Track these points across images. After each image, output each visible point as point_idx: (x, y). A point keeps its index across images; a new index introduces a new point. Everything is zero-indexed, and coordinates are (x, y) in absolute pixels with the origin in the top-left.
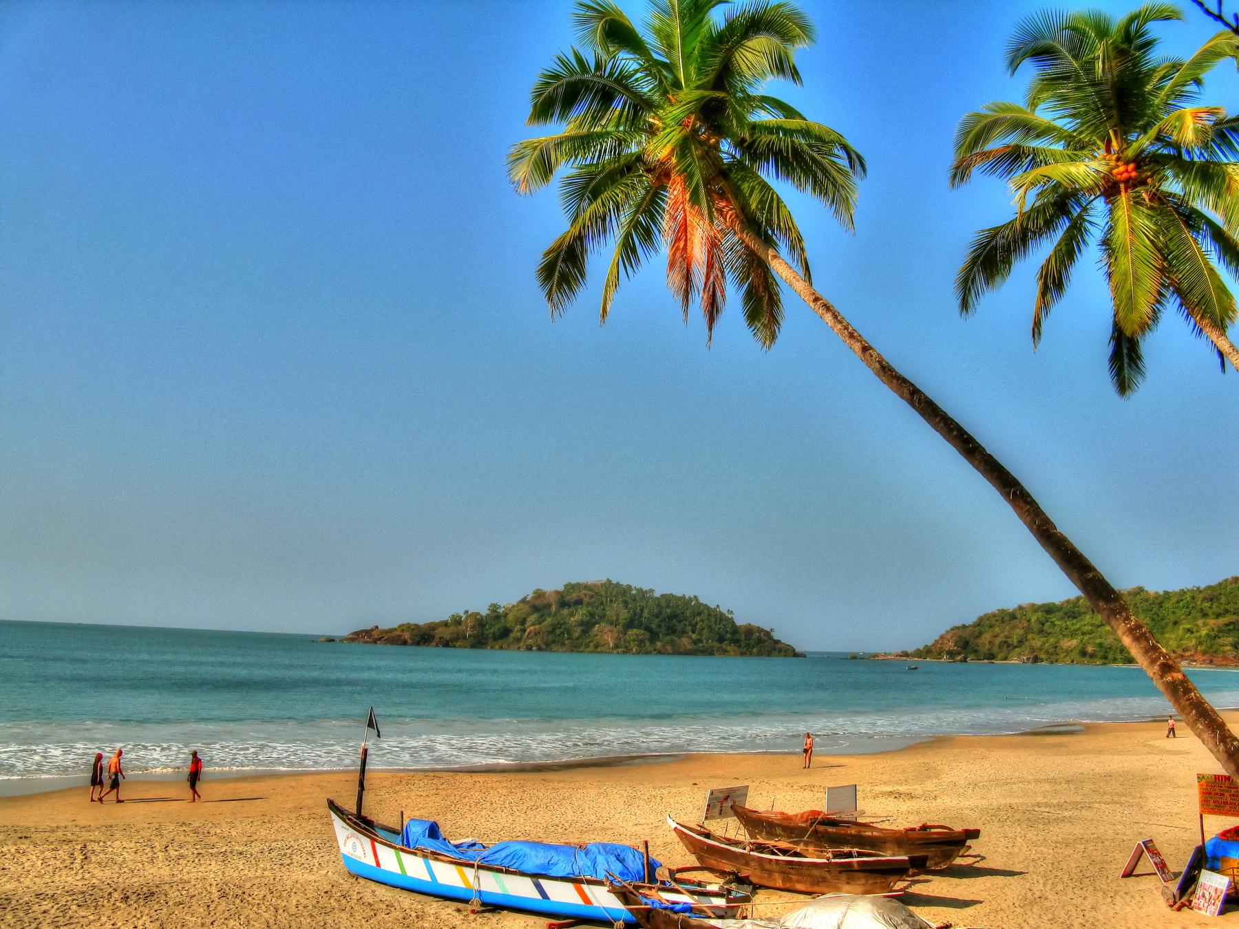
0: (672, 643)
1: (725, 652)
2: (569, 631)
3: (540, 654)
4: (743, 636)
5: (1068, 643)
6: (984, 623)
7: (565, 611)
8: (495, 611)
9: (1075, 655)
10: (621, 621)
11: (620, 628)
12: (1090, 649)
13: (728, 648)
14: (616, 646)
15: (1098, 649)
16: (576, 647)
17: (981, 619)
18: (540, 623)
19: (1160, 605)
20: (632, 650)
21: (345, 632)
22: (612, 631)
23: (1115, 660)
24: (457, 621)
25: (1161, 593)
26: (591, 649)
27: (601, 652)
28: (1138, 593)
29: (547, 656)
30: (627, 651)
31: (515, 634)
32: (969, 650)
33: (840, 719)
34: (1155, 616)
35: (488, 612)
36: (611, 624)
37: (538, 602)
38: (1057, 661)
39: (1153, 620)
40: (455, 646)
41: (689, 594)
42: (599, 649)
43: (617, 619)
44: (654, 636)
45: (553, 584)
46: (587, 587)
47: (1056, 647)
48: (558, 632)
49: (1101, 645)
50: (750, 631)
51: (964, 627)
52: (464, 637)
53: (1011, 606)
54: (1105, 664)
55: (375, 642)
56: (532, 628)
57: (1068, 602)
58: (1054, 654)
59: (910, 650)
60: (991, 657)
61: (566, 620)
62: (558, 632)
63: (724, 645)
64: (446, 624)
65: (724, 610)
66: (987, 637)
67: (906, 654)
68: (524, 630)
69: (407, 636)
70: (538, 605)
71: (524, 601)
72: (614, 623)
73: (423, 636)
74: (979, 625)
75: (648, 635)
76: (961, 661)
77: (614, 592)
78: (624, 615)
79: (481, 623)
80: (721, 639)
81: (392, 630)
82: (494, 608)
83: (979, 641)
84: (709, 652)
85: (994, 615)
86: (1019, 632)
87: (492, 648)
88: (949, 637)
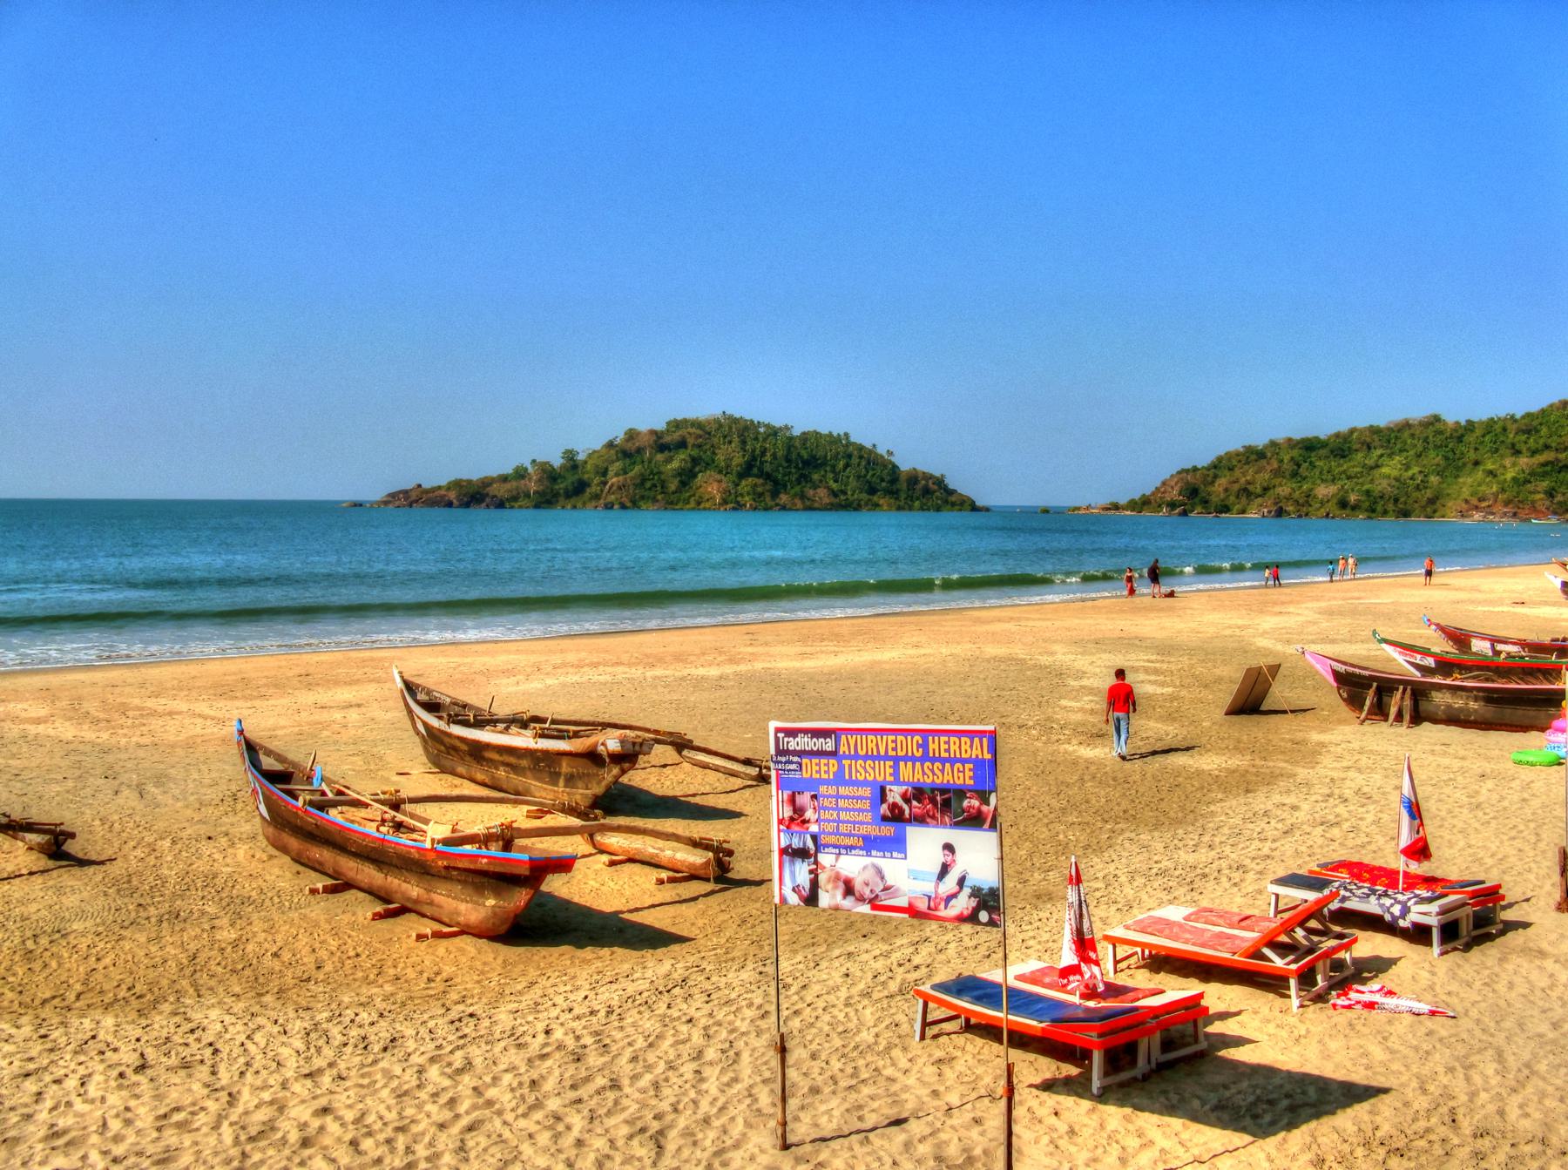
0: (803, 497)
1: (876, 506)
2: (663, 484)
3: (623, 513)
4: (904, 486)
5: (1323, 491)
6: (1220, 465)
7: (660, 457)
8: (572, 459)
9: (1332, 507)
10: (736, 469)
11: (733, 477)
12: (1353, 498)
13: (881, 502)
14: (725, 502)
15: (1363, 498)
16: (672, 503)
17: (1220, 459)
18: (626, 473)
19: (1460, 439)
20: (745, 505)
21: (376, 493)
22: (720, 481)
23: (1385, 513)
24: (521, 474)
25: (1463, 423)
26: (692, 504)
27: (705, 509)
28: (1432, 424)
29: (631, 514)
30: (739, 507)
31: (594, 489)
32: (1197, 500)
33: (436, 590)
34: (1450, 455)
35: (562, 461)
36: (720, 472)
37: (630, 446)
38: (1307, 515)
39: (1447, 458)
40: (512, 507)
41: (837, 430)
42: (702, 506)
43: (728, 466)
44: (777, 487)
45: (651, 417)
46: (697, 424)
47: (1308, 496)
48: (648, 485)
49: (1368, 493)
50: (914, 478)
51: (1195, 469)
52: (527, 495)
53: (1260, 441)
54: (1369, 518)
55: (411, 506)
56: (614, 480)
57: (1337, 435)
58: (1304, 506)
59: (1123, 501)
60: (1225, 509)
61: (662, 469)
62: (648, 485)
63: (875, 498)
64: (504, 479)
65: (882, 450)
66: (1222, 482)
67: (1116, 507)
68: (605, 483)
69: (452, 495)
70: (627, 451)
71: (610, 445)
72: (725, 470)
73: (473, 495)
74: (1215, 467)
75: (769, 486)
76: (1180, 514)
77: (742, 430)
78: (738, 460)
79: (549, 474)
80: (872, 491)
81: (433, 490)
82: (570, 455)
83: (1211, 489)
84: (857, 507)
85: (1238, 454)
86: (1265, 476)
87: (563, 507)
88: (1173, 483)
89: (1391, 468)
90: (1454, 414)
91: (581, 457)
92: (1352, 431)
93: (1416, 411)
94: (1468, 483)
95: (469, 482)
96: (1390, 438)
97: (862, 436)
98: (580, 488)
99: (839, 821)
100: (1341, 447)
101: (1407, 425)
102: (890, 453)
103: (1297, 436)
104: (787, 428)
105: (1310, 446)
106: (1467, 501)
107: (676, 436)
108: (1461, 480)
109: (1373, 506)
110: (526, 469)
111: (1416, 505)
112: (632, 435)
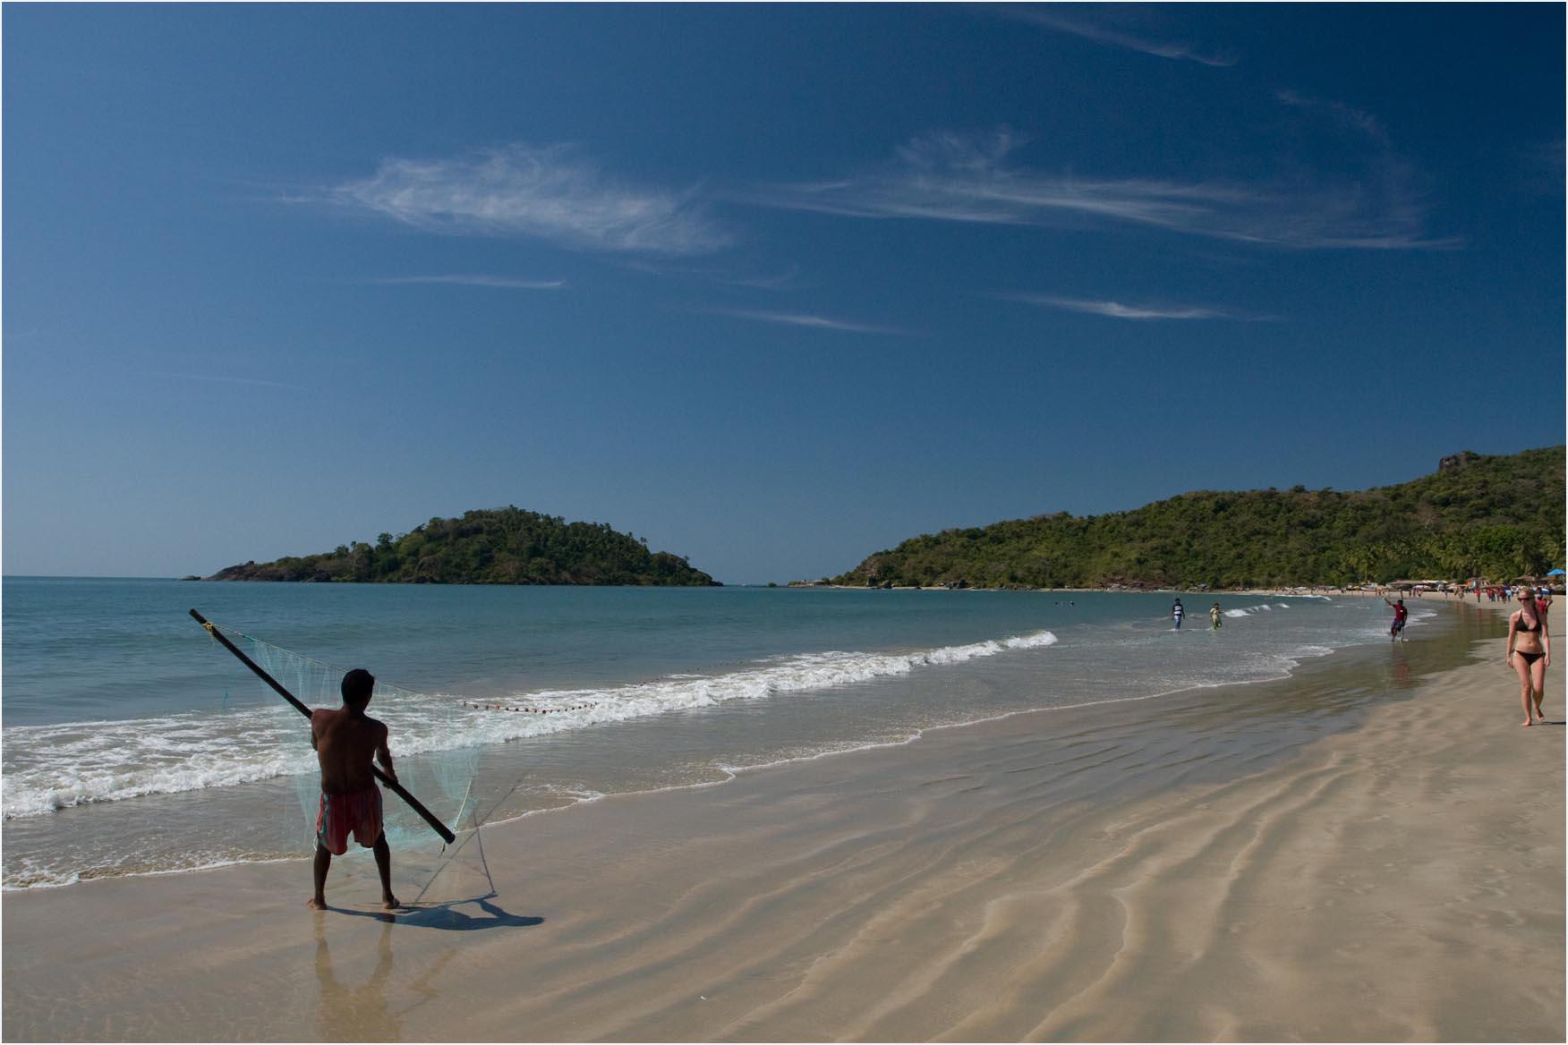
6: (905, 549)
8: (387, 542)
9: (1004, 579)
17: (904, 545)
24: (342, 552)
35: (378, 543)
39: (1079, 544)
46: (489, 515)
64: (329, 557)
65: (636, 537)
66: (912, 560)
68: (416, 562)
70: (436, 533)
71: (419, 530)
74: (901, 551)
77: (517, 520)
79: (367, 554)
81: (265, 566)
82: (385, 538)
89: (1040, 552)
90: (1079, 512)
91: (394, 541)
92: (1002, 524)
93: (1051, 509)
94: (1101, 562)
95: (297, 560)
96: (1036, 528)
97: (621, 528)
98: (393, 566)
99: (384, 699)
100: (998, 535)
101: (1044, 520)
102: (643, 540)
103: (963, 527)
104: (560, 519)
105: (974, 535)
106: (1104, 576)
107: (475, 523)
108: (1093, 560)
109: (1037, 578)
110: (347, 549)
111: (1066, 579)
112: (436, 523)
